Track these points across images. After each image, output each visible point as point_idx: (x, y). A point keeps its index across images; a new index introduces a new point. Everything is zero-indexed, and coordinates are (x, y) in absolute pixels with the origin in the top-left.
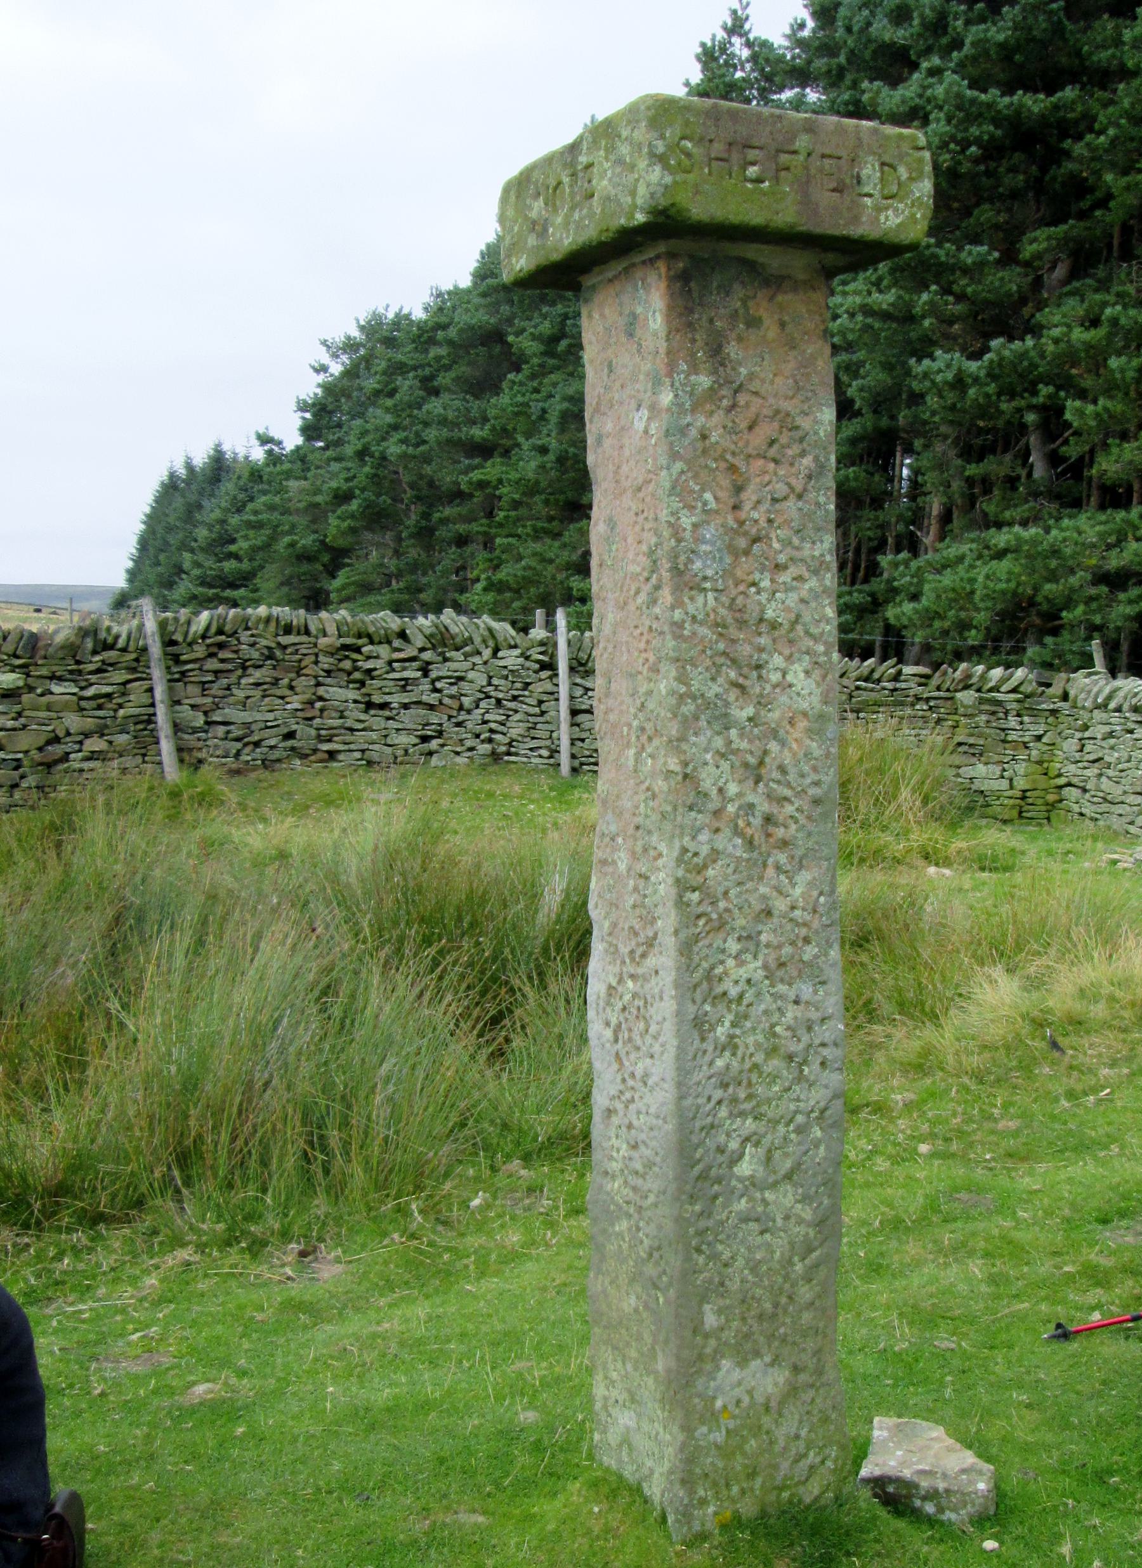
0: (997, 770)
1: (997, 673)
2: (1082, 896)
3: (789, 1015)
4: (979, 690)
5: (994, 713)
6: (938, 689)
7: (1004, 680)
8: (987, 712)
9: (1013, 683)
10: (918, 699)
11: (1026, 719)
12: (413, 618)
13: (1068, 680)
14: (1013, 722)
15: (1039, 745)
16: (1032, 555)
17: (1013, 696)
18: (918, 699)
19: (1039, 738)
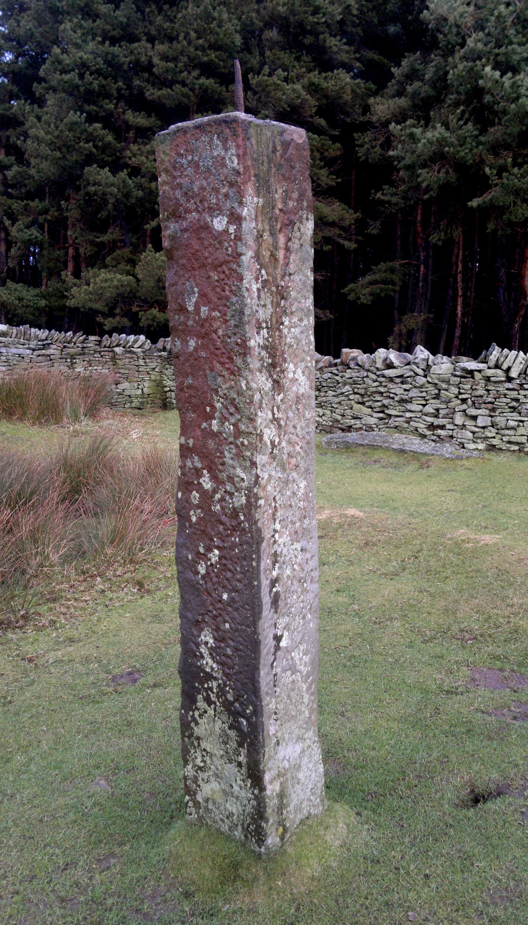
0: (136, 385)
1: (132, 338)
2: (100, 443)
3: (300, 557)
4: (124, 347)
5: (132, 358)
6: (105, 347)
7: (135, 341)
8: (129, 358)
9: (139, 343)
10: (95, 352)
11: (147, 361)
12: (332, 71)
13: (165, 341)
14: (141, 362)
15: (154, 373)
16: (458, 243)
17: (140, 350)
18: (95, 352)
19: (154, 369)
